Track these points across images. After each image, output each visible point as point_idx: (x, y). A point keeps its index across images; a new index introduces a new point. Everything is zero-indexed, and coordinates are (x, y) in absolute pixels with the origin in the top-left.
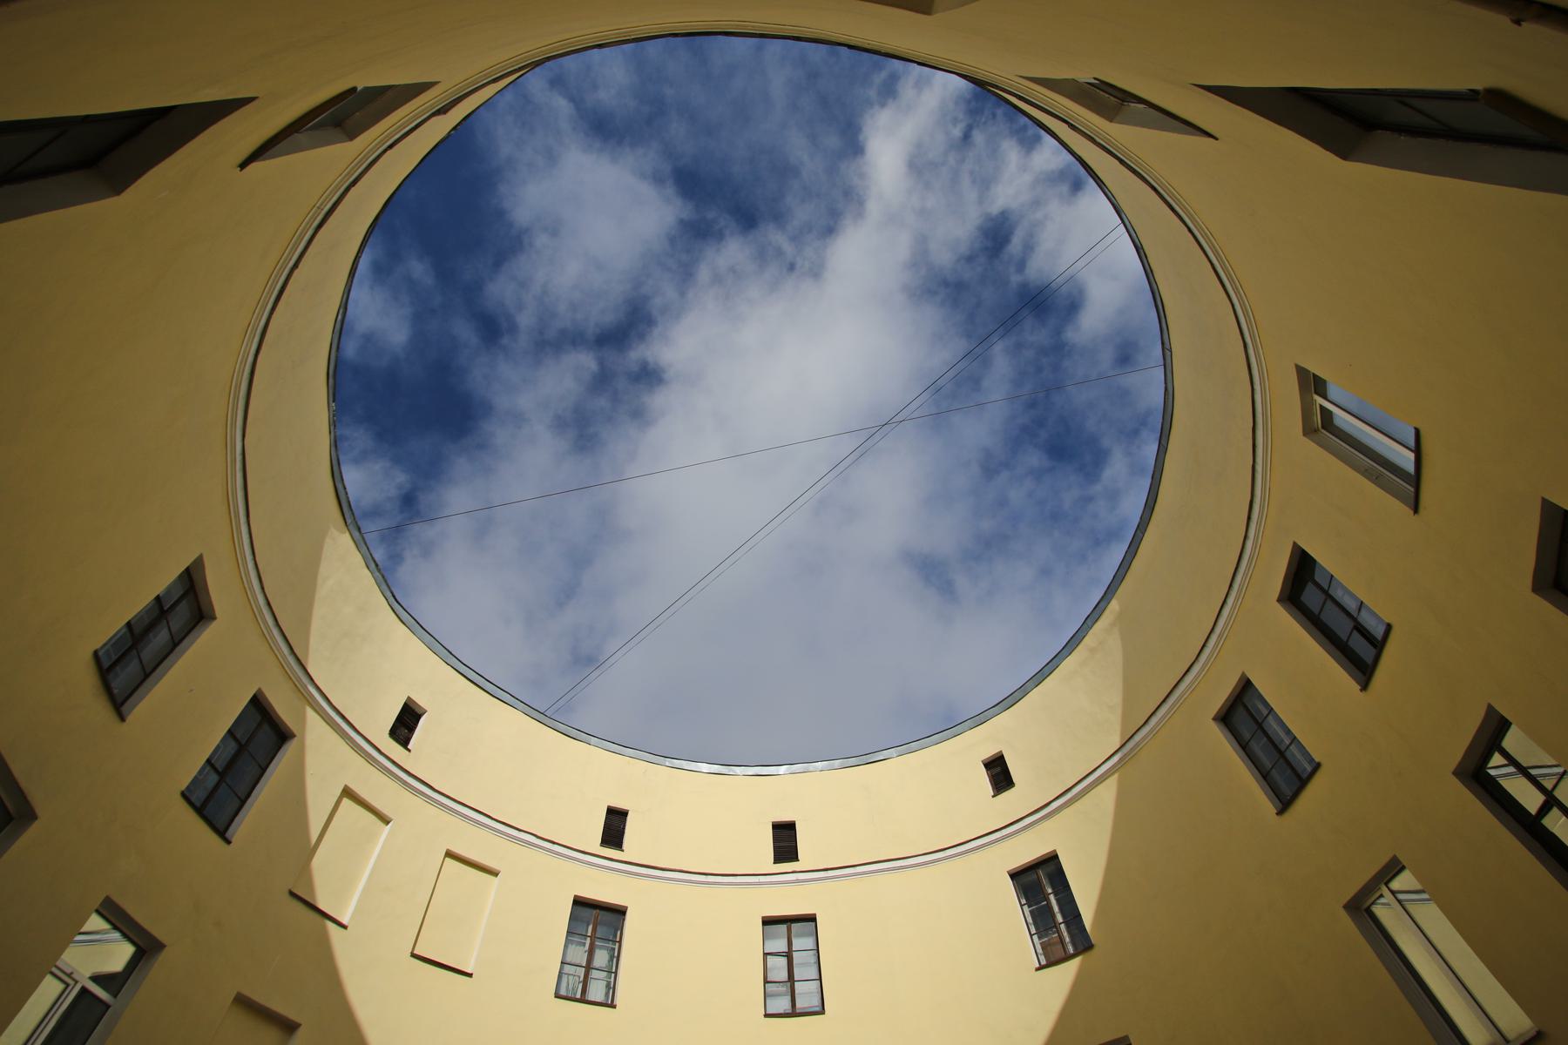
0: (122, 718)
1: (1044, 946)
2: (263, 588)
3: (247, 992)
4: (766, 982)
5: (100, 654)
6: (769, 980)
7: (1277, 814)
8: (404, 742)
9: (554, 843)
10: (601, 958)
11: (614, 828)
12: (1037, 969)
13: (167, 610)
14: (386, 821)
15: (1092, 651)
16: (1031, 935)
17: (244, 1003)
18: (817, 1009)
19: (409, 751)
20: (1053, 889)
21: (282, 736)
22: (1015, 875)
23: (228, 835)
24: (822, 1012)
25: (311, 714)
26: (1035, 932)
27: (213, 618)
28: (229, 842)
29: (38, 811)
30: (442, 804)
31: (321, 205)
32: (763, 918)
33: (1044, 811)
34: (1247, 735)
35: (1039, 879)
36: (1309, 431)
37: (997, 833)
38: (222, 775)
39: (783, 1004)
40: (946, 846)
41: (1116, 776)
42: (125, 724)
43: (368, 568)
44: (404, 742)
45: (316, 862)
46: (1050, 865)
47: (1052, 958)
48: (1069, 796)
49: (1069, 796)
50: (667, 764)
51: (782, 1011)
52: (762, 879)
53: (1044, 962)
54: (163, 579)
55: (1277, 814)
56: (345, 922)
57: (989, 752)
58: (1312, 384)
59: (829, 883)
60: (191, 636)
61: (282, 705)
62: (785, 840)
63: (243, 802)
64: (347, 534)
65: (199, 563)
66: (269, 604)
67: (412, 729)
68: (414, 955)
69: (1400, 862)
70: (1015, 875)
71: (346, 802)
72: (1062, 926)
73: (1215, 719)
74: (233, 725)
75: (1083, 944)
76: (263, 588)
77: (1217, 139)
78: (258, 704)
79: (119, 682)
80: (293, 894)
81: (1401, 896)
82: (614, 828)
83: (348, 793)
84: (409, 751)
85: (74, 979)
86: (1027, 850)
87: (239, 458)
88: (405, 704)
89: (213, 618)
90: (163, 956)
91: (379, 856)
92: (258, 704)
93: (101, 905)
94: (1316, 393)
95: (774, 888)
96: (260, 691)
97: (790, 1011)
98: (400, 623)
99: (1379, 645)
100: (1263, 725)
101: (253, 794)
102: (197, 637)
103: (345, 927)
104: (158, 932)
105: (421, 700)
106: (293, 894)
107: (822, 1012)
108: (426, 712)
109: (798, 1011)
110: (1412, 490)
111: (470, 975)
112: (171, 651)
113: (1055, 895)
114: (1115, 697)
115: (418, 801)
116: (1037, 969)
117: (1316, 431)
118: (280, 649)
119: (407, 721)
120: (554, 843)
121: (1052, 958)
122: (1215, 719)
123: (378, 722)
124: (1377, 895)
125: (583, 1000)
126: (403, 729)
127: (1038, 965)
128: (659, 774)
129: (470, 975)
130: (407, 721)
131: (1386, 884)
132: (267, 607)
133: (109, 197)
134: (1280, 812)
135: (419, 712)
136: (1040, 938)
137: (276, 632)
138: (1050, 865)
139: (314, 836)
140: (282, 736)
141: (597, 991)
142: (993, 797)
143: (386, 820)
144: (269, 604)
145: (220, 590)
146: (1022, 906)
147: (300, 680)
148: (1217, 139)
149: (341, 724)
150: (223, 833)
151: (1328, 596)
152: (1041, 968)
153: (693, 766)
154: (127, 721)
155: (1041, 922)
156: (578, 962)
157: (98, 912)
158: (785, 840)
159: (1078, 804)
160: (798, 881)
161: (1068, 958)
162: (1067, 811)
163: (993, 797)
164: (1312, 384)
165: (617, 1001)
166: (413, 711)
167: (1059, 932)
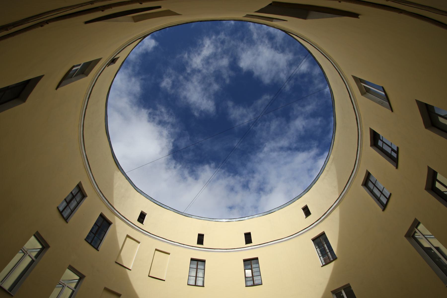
0: (67, 222)
1: (320, 251)
2: (98, 188)
3: (107, 287)
4: (246, 277)
5: (73, 193)
6: (246, 276)
7: (382, 211)
8: (142, 222)
9: (184, 245)
10: (200, 274)
11: (201, 239)
12: (322, 266)
13: (75, 196)
14: (139, 243)
15: (328, 171)
16: (320, 257)
17: (106, 289)
18: (261, 284)
19: (143, 224)
20: (325, 242)
21: (109, 224)
22: (314, 240)
23: (98, 249)
24: (262, 284)
25: (116, 218)
26: (321, 255)
27: (87, 196)
28: (98, 251)
29: (50, 245)
30: (153, 237)
31: (87, 92)
32: (243, 260)
33: (320, 220)
34: (372, 188)
35: (320, 240)
36: (363, 94)
37: (307, 229)
38: (95, 234)
39: (251, 283)
40: (293, 234)
41: (338, 207)
42: (68, 224)
43: (127, 179)
44: (142, 222)
45: (122, 254)
46: (323, 235)
47: (327, 262)
48: (326, 215)
49: (326, 215)
50: (214, 221)
51: (251, 285)
52: (242, 249)
53: (324, 264)
54: (72, 187)
55: (382, 211)
56: (130, 268)
57: (303, 206)
58: (358, 81)
59: (261, 248)
60: (82, 202)
61: (109, 216)
62: (248, 238)
63: (101, 241)
64: (120, 172)
65: (80, 183)
66: (101, 191)
67: (144, 219)
68: (149, 276)
69: (418, 221)
70: (314, 240)
71: (128, 239)
72: (329, 253)
73: (362, 185)
74: (96, 221)
75: (335, 258)
76: (98, 188)
77: (287, 21)
78: (102, 216)
79: (66, 214)
80: (116, 262)
81: (426, 236)
82: (201, 239)
83: (128, 236)
84: (143, 224)
85: (65, 285)
86: (316, 232)
87: (85, 157)
88: (141, 212)
89: (87, 196)
90: (85, 279)
91: (138, 252)
92: (102, 216)
93: (68, 267)
94: (361, 82)
95: (246, 251)
96: (102, 213)
97: (253, 285)
98: (137, 192)
99: (397, 152)
100: (381, 193)
101: (100, 245)
102: (83, 202)
103: (130, 270)
104: (83, 273)
105: (145, 211)
106: (116, 262)
107: (262, 284)
108: (147, 214)
109: (255, 284)
110: (388, 103)
111: (164, 280)
112: (78, 205)
113: (326, 245)
114: (335, 183)
115: (147, 237)
116: (322, 266)
117: (365, 93)
118: (105, 202)
119: (142, 218)
120: (184, 245)
121: (327, 262)
122: (362, 185)
123: (134, 218)
124: (414, 231)
125: (195, 285)
126: (141, 219)
127: (322, 265)
128: (212, 224)
129: (164, 280)
130: (142, 218)
131: (417, 227)
132: (100, 192)
133: (113, 64)
134: (384, 210)
135: (145, 214)
136: (323, 258)
137: (104, 198)
138: (323, 235)
139: (120, 248)
140: (109, 224)
141: (200, 283)
142: (305, 218)
143: (139, 243)
144: (101, 191)
145: (87, 188)
146: (316, 249)
147: (112, 209)
148: (287, 21)
149: (124, 219)
150: (97, 249)
151: (384, 142)
152: (323, 266)
153: (221, 220)
154: (69, 223)
155: (323, 253)
156: (195, 268)
157: (68, 268)
158: (248, 238)
159: (329, 217)
160: (252, 249)
161: (331, 262)
162: (326, 219)
163: (305, 218)
164: (358, 81)
165: (205, 285)
166: (143, 214)
167: (328, 255)
